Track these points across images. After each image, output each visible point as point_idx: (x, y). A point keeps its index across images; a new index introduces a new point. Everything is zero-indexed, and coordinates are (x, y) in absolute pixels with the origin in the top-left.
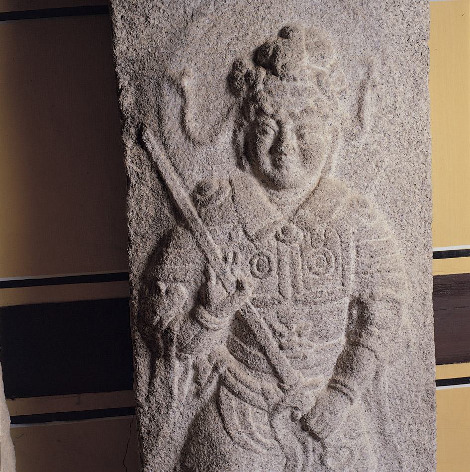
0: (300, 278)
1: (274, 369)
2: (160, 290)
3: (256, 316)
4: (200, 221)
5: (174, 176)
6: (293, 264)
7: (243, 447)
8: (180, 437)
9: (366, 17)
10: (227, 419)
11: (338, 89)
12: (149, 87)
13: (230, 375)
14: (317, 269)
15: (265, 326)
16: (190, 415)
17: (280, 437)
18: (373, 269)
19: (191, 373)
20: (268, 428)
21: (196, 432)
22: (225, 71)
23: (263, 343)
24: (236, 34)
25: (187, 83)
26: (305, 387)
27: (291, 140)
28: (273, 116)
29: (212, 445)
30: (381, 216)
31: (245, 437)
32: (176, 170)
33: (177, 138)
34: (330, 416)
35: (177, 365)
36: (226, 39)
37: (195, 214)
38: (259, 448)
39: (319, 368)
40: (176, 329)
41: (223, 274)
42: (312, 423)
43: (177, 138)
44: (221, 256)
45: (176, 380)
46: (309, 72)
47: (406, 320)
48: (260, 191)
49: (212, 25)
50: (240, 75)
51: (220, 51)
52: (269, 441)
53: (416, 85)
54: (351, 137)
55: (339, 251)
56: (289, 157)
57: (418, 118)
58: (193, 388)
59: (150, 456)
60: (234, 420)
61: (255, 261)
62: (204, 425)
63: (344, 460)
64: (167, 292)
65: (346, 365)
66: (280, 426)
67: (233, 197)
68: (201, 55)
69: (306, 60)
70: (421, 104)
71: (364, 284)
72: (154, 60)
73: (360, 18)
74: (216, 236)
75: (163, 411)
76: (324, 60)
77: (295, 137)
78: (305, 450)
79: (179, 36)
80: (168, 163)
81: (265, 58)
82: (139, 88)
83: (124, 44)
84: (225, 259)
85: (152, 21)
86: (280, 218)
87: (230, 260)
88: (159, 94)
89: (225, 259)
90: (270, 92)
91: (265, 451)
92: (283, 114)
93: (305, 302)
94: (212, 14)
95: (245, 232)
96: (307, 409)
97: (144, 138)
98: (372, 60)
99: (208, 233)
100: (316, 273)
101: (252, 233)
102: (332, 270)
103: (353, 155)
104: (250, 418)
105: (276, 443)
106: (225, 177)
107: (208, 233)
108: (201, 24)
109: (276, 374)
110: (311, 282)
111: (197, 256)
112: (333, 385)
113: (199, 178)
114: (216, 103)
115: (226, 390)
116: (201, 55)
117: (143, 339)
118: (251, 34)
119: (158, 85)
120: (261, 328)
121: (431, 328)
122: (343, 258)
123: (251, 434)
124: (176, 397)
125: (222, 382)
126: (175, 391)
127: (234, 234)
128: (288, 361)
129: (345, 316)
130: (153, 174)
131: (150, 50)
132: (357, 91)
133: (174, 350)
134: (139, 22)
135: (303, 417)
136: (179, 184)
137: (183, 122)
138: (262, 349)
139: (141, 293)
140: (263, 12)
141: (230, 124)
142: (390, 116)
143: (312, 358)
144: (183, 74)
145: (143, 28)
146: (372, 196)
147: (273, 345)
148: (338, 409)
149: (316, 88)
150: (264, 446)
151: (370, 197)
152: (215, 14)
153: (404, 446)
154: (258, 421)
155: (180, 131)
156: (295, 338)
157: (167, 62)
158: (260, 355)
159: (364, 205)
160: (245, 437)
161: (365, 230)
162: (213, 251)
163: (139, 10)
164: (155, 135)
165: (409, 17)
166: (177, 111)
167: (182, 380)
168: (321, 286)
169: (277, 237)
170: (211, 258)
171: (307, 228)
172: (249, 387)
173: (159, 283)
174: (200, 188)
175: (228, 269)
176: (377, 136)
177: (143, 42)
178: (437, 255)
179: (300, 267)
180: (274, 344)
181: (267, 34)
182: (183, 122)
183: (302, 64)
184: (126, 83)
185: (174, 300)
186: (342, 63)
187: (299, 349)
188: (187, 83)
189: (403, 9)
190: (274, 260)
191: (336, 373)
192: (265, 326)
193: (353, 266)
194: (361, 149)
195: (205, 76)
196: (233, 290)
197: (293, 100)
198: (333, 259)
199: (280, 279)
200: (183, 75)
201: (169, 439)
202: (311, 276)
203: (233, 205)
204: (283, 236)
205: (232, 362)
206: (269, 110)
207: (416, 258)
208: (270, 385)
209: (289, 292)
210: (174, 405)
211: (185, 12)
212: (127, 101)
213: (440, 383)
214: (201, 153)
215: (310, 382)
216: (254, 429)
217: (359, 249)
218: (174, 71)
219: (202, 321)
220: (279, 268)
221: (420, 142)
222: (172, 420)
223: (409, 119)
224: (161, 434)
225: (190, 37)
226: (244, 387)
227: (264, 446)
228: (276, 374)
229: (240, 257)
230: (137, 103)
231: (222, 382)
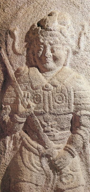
0: (52, 104)
4: (17, 82)
5: (10, 66)
9: (83, 8)
10: (24, 158)
13: (26, 141)
14: (58, 101)
16: (12, 156)
20: (39, 163)
21: (14, 161)
24: (34, 15)
32: (11, 64)
33: (11, 52)
34: (63, 160)
36: (30, 17)
39: (61, 141)
43: (11, 52)
45: (8, 142)
49: (26, 12)
51: (28, 21)
52: (39, 168)
56: (49, 59)
60: (26, 159)
67: (28, 73)
68: (21, 23)
69: (56, 23)
72: (6, 24)
73: (80, 8)
74: (22, 87)
75: (3, 153)
76: (64, 23)
79: (15, 16)
81: (42, 24)
88: (6, 37)
89: (24, 95)
91: (38, 172)
94: (26, 8)
98: (85, 24)
99: (19, 86)
100: (58, 103)
103: (77, 59)
107: (19, 86)
108: (22, 11)
116: (21, 23)
118: (39, 15)
119: (6, 34)
122: (69, 98)
124: (7, 148)
126: (7, 146)
128: (47, 137)
131: (4, 21)
132: (78, 35)
134: (1, 11)
136: (11, 69)
140: (44, 7)
145: (2, 14)
148: (67, 158)
150: (37, 170)
152: (27, 8)
154: (35, 160)
156: (50, 127)
157: (10, 25)
161: (78, 87)
162: (20, 93)
163: (1, 7)
164: (5, 51)
166: (12, 42)
167: (10, 142)
168: (60, 108)
169: (43, 89)
175: (25, 100)
177: (2, 18)
179: (52, 100)
181: (44, 15)
183: (54, 25)
185: (7, 110)
186: (73, 25)
187: (52, 132)
188: (16, 33)
190: (42, 97)
191: (67, 144)
194: (80, 57)
199: (44, 104)
200: (14, 29)
201: (4, 165)
202: (56, 104)
203: (28, 76)
209: (48, 110)
210: (7, 151)
211: (17, 8)
217: (75, 94)
218: (12, 28)
225: (18, 16)
226: (31, 146)
227: (37, 170)
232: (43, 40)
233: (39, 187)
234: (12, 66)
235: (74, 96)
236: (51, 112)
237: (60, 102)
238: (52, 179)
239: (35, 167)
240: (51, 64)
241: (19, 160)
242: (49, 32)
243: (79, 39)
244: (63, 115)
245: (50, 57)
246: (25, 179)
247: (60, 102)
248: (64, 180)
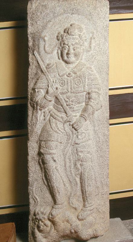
0: (72, 86)
1: (65, 112)
2: (36, 91)
3: (61, 97)
4: (47, 72)
7: (56, 132)
8: (39, 132)
10: (51, 125)
11: (85, 39)
12: (36, 40)
15: (63, 99)
17: (66, 130)
18: (92, 84)
19: (43, 114)
20: (63, 127)
21: (44, 129)
22: (56, 35)
23: (62, 104)
25: (46, 38)
26: (73, 116)
27: (72, 51)
28: (67, 45)
29: (47, 132)
30: (95, 72)
31: (56, 129)
33: (42, 52)
35: (39, 112)
37: (46, 71)
38: (60, 132)
40: (39, 101)
41: (52, 86)
42: (75, 126)
44: (52, 81)
45: (39, 116)
46: (77, 34)
47: (101, 99)
48: (63, 64)
50: (60, 35)
53: (105, 38)
55: (83, 79)
57: (105, 47)
58: (43, 118)
59: (31, 138)
60: (54, 125)
61: (61, 82)
62: (46, 127)
64: (38, 92)
66: (66, 127)
69: (76, 31)
70: (106, 43)
75: (35, 125)
77: (73, 50)
78: (73, 133)
79: (44, 27)
80: (40, 59)
81: (66, 31)
82: (34, 41)
83: (30, 29)
84: (53, 82)
85: (38, 23)
86: (68, 71)
87: (55, 82)
89: (53, 82)
90: (67, 39)
91: (61, 133)
92: (70, 44)
93: (74, 93)
95: (59, 74)
96: (73, 122)
97: (34, 53)
100: (77, 85)
101: (60, 75)
105: (65, 131)
106: (54, 62)
109: (66, 113)
110: (75, 87)
111: (46, 81)
112: (81, 116)
113: (48, 62)
114: (53, 43)
115: (52, 118)
117: (31, 106)
119: (39, 40)
120: (62, 100)
121: (108, 102)
122: (84, 81)
123: (58, 129)
124: (38, 120)
125: (51, 115)
126: (38, 119)
127: (56, 75)
128: (69, 109)
129: (85, 97)
130: (36, 62)
133: (39, 107)
135: (72, 124)
137: (44, 48)
138: (62, 106)
139: (31, 93)
141: (57, 48)
143: (76, 108)
144: (45, 36)
146: (93, 67)
147: (65, 104)
149: (79, 38)
150: (61, 132)
151: (92, 67)
153: (100, 134)
154: (60, 126)
155: (43, 51)
156: (71, 102)
158: (61, 107)
159: (91, 68)
160: (56, 129)
162: (50, 80)
164: (37, 52)
165: (104, 21)
166: (43, 46)
170: (49, 82)
172: (58, 116)
173: (36, 89)
174: (48, 65)
176: (95, 51)
178: (110, 89)
180: (65, 104)
181: (67, 25)
182: (44, 48)
184: (31, 39)
187: (72, 106)
189: (102, 19)
190: (66, 81)
192: (63, 99)
195: (51, 36)
196: (55, 90)
197: (72, 40)
198: (81, 81)
201: (36, 133)
204: (69, 75)
205: (54, 110)
206: (66, 43)
208: (64, 115)
209: (70, 90)
212: (30, 44)
213: (111, 125)
214: (49, 56)
215: (75, 116)
216: (59, 127)
219: (46, 98)
220: (67, 83)
221: (106, 53)
222: (37, 127)
223: (103, 47)
224: (34, 131)
228: (66, 113)
229: (57, 81)
230: (33, 45)
231: (51, 115)
232: (67, 42)
233: (62, 144)
234: (43, 62)
235: (83, 197)
236: (72, 91)
237: (78, 84)
238: (71, 137)
239: (60, 131)
240: (72, 58)
241: (48, 126)
242: (71, 37)
243: (91, 41)
244: (59, 116)
245: (72, 54)
246: (53, 139)
247: (78, 84)
248: (79, 137)
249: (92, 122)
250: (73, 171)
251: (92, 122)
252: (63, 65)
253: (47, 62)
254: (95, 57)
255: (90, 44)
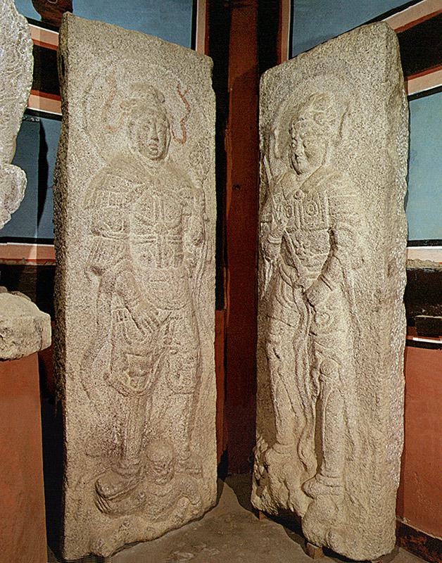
6: (300, 210)
26: (307, 276)
38: (286, 305)
47: (361, 241)
54: (336, 144)
55: (319, 202)
63: (325, 321)
65: (327, 267)
71: (333, 221)
102: (318, 213)
104: (285, 289)
123: (283, 297)
142: (359, 129)
171: (306, 192)
193: (327, 210)
207: (372, 208)
212: (261, 146)
215: (310, 275)
248: (318, 320)
249: (346, 293)
250: (309, 387)
251: (346, 293)
252: (356, 193)
253: (276, 173)
254: (351, 153)
255: (341, 129)
